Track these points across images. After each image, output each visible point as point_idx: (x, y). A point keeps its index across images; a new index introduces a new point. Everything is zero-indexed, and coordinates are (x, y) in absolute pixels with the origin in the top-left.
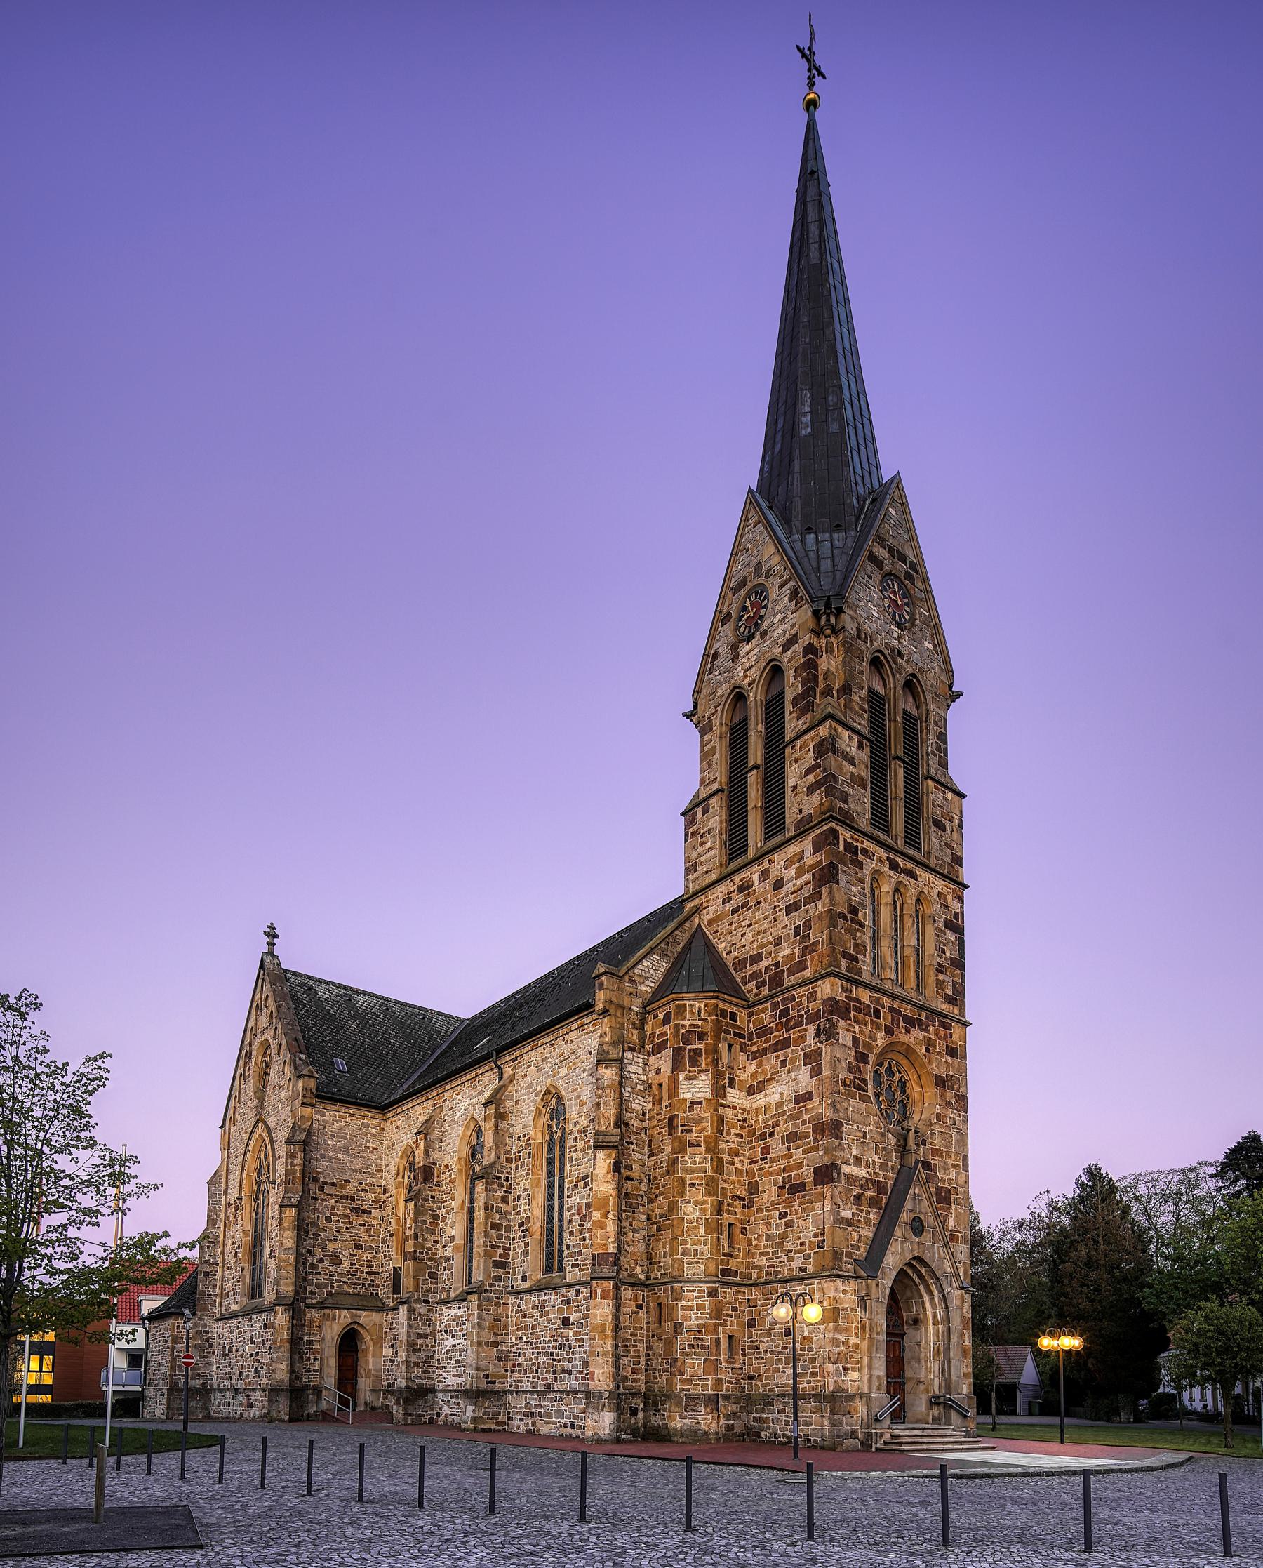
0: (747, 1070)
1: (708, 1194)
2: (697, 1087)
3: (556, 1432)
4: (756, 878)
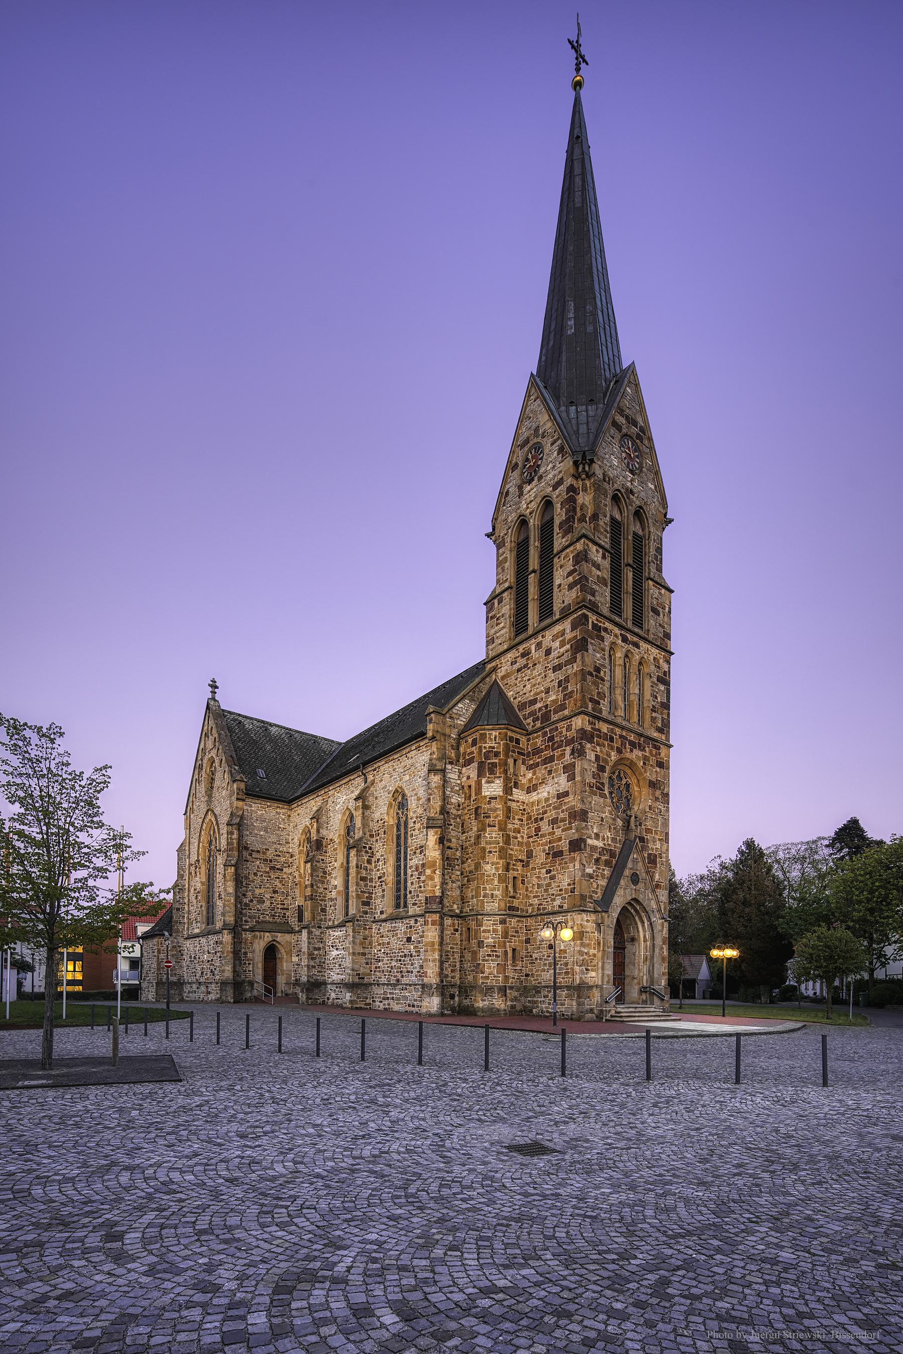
1: (500, 858)
2: (493, 788)
4: (533, 647)
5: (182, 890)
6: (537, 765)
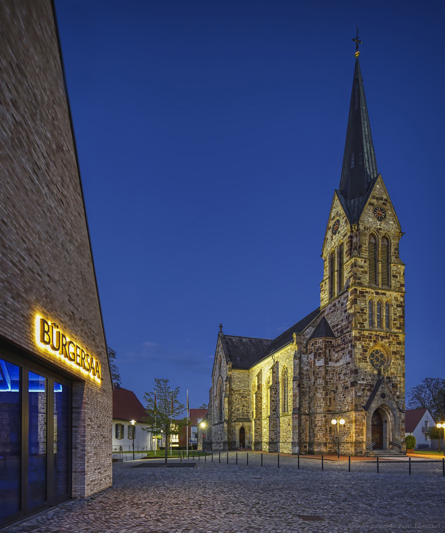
0: (335, 356)
1: (323, 390)
2: (320, 363)
3: (287, 452)
4: (337, 303)
5: (211, 406)
6: (339, 351)
